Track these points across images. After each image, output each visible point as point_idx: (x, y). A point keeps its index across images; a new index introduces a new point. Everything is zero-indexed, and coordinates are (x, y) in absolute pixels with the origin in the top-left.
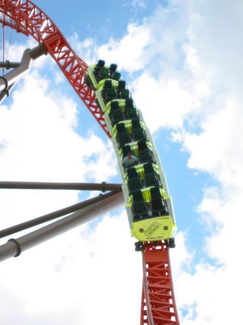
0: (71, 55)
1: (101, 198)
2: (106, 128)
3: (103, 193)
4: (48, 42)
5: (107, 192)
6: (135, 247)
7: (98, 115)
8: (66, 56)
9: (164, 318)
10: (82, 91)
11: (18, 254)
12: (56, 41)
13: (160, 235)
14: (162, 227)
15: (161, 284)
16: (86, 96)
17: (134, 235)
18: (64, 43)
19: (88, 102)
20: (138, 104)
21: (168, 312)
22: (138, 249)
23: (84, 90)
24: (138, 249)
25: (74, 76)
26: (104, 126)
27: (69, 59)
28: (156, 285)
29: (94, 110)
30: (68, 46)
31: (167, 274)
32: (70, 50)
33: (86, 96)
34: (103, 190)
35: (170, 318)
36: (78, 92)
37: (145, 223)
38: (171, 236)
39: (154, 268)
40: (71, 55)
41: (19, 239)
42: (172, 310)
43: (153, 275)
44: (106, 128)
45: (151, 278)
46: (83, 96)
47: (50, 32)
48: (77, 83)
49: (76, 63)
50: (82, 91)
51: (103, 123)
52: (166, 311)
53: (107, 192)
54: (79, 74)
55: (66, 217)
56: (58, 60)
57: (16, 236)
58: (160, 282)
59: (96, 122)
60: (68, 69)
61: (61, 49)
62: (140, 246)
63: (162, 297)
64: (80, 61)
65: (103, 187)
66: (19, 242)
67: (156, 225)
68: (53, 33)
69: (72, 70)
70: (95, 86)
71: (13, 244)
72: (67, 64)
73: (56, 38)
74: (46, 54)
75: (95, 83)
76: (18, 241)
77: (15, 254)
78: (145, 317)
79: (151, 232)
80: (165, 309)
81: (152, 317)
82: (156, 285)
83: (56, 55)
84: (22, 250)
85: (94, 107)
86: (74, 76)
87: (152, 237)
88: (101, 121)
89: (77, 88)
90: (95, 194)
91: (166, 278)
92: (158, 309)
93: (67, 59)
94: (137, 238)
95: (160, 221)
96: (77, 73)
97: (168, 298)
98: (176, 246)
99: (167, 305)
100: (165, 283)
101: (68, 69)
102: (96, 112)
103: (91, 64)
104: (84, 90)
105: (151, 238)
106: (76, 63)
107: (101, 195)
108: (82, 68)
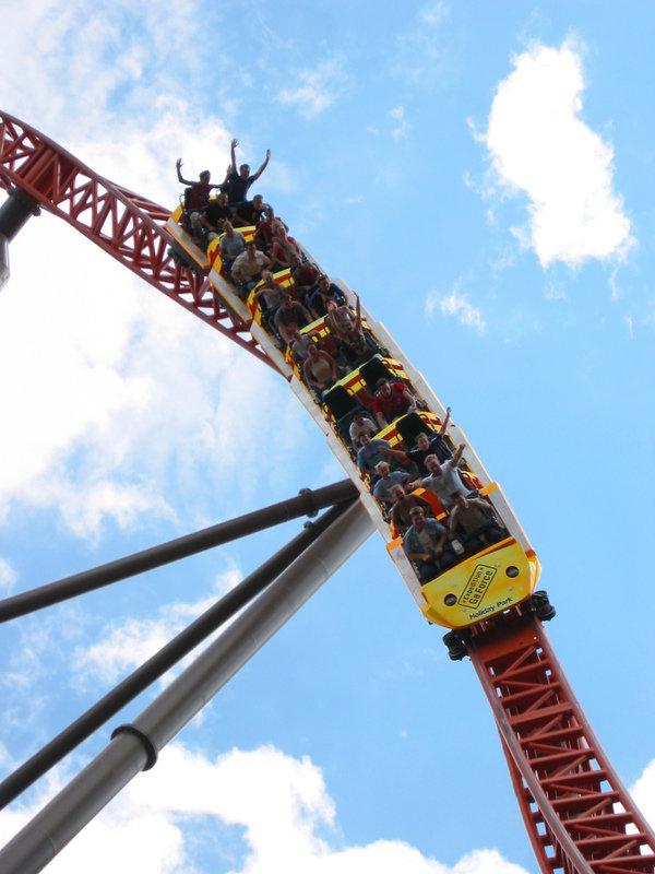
0: (102, 191)
1: (312, 532)
2: (258, 347)
3: (313, 520)
4: (30, 182)
5: (322, 512)
6: (446, 649)
7: (227, 323)
8: (90, 200)
9: (603, 835)
10: (164, 273)
11: (151, 761)
12: (51, 170)
13: (500, 598)
14: (502, 572)
15: (544, 705)
16: (177, 284)
17: (434, 616)
18: (71, 166)
19: (189, 298)
20: (332, 267)
21: (587, 774)
22: (457, 654)
23: (169, 269)
24: (457, 654)
25: (130, 243)
26: (251, 346)
27: (100, 205)
28: (531, 714)
29: (210, 312)
30: (86, 172)
31: (548, 673)
32: (96, 179)
33: (217, 311)
34: (312, 513)
35: (623, 831)
36: (155, 280)
37: (454, 579)
38: (535, 588)
39: (507, 673)
40: (102, 191)
41: (144, 718)
42: (618, 809)
43: (514, 690)
44: (258, 347)
45: (512, 702)
46: (170, 286)
47: (27, 152)
48: (145, 258)
49: (121, 208)
50: (164, 273)
51: (246, 336)
52: (581, 773)
53: (322, 512)
54: (140, 232)
55: (252, 606)
56: (72, 218)
57: (129, 714)
58: (540, 701)
59: (209, 328)
60: (107, 230)
61: (71, 184)
62: (460, 642)
63: (555, 741)
64: (129, 199)
65: (305, 503)
66: (144, 729)
67: (484, 572)
68: (35, 151)
69: (119, 229)
70: (202, 264)
71: (131, 741)
72: (99, 220)
73: (47, 160)
74: (37, 213)
75: (201, 258)
76: (139, 728)
77: (144, 760)
78: (541, 829)
79: (476, 596)
80: (577, 771)
81: (549, 804)
82: (531, 714)
83: (65, 206)
84: (158, 746)
85: (207, 304)
86: (130, 243)
87: (482, 608)
88: (241, 335)
89: (149, 272)
90: (294, 528)
91: (550, 685)
92: (558, 777)
93: (93, 205)
94: (445, 623)
95: (493, 559)
96: (75, 192)
97: (594, 781)
98: (556, 609)
99: (577, 757)
100: (553, 701)
101: (107, 230)
102: (218, 316)
103: (170, 198)
104: (169, 269)
105: (481, 613)
106: (121, 208)
107: (308, 525)
108: (142, 216)
